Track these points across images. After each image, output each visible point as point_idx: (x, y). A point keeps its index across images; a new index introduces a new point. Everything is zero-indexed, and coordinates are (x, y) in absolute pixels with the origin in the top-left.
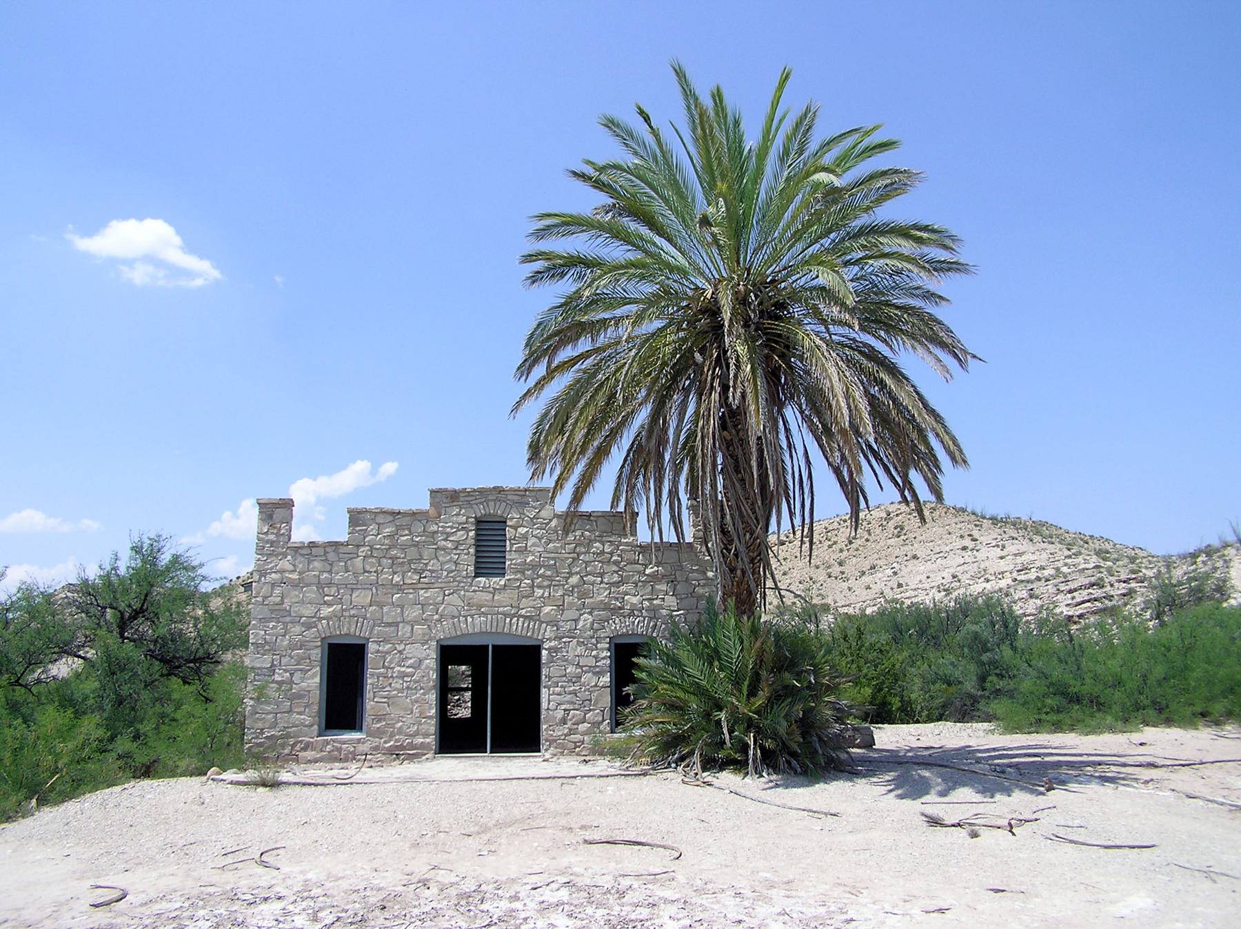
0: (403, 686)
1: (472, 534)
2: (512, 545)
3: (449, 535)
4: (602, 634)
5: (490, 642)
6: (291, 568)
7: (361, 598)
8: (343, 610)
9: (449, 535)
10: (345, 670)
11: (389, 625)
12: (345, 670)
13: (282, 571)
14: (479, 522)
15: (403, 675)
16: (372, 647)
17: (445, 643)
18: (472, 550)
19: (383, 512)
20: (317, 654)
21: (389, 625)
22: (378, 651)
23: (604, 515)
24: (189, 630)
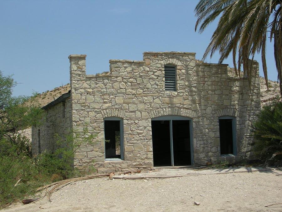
0: (139, 140)
1: (164, 72)
2: (179, 77)
3: (154, 72)
4: (216, 115)
5: (171, 119)
6: (89, 87)
7: (119, 100)
8: (112, 106)
9: (154, 72)
10: (113, 129)
11: (132, 112)
12: (113, 129)
13: (85, 88)
14: (166, 67)
15: (139, 134)
16: (125, 122)
17: (121, 122)
18: (164, 79)
19: (127, 62)
20: (102, 125)
21: (132, 112)
22: (128, 124)
23: (215, 66)
24: (212, 135)
